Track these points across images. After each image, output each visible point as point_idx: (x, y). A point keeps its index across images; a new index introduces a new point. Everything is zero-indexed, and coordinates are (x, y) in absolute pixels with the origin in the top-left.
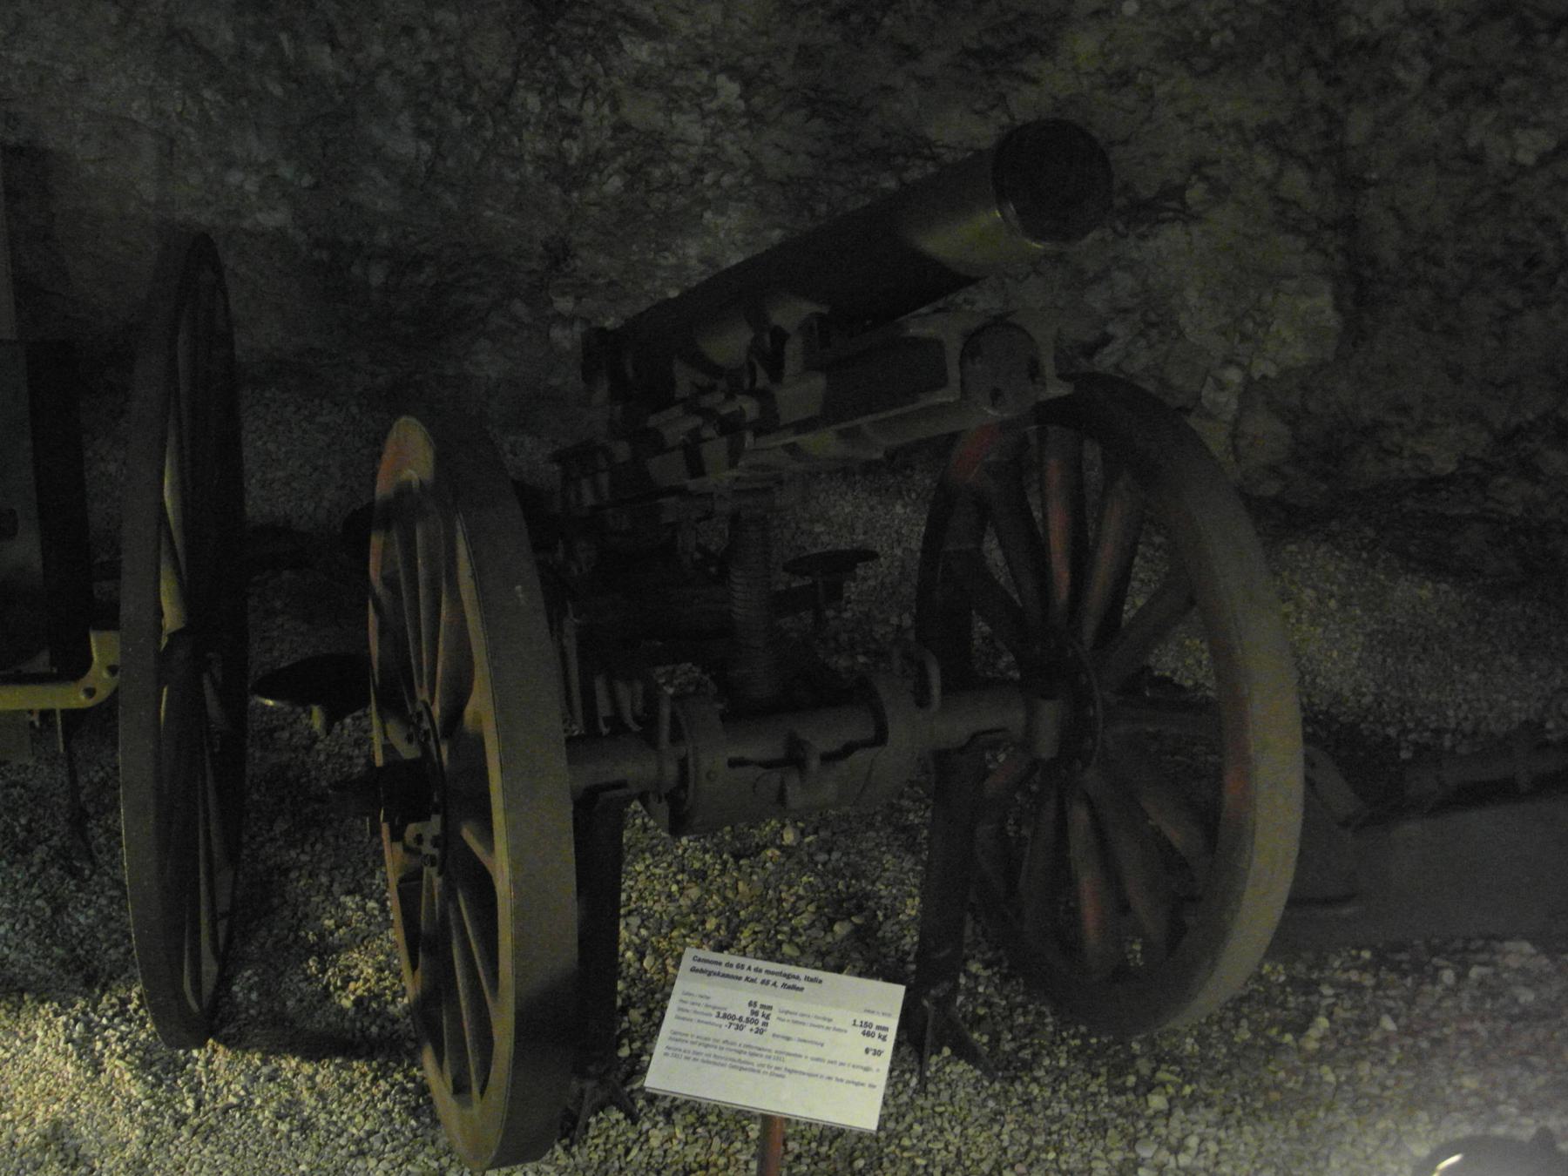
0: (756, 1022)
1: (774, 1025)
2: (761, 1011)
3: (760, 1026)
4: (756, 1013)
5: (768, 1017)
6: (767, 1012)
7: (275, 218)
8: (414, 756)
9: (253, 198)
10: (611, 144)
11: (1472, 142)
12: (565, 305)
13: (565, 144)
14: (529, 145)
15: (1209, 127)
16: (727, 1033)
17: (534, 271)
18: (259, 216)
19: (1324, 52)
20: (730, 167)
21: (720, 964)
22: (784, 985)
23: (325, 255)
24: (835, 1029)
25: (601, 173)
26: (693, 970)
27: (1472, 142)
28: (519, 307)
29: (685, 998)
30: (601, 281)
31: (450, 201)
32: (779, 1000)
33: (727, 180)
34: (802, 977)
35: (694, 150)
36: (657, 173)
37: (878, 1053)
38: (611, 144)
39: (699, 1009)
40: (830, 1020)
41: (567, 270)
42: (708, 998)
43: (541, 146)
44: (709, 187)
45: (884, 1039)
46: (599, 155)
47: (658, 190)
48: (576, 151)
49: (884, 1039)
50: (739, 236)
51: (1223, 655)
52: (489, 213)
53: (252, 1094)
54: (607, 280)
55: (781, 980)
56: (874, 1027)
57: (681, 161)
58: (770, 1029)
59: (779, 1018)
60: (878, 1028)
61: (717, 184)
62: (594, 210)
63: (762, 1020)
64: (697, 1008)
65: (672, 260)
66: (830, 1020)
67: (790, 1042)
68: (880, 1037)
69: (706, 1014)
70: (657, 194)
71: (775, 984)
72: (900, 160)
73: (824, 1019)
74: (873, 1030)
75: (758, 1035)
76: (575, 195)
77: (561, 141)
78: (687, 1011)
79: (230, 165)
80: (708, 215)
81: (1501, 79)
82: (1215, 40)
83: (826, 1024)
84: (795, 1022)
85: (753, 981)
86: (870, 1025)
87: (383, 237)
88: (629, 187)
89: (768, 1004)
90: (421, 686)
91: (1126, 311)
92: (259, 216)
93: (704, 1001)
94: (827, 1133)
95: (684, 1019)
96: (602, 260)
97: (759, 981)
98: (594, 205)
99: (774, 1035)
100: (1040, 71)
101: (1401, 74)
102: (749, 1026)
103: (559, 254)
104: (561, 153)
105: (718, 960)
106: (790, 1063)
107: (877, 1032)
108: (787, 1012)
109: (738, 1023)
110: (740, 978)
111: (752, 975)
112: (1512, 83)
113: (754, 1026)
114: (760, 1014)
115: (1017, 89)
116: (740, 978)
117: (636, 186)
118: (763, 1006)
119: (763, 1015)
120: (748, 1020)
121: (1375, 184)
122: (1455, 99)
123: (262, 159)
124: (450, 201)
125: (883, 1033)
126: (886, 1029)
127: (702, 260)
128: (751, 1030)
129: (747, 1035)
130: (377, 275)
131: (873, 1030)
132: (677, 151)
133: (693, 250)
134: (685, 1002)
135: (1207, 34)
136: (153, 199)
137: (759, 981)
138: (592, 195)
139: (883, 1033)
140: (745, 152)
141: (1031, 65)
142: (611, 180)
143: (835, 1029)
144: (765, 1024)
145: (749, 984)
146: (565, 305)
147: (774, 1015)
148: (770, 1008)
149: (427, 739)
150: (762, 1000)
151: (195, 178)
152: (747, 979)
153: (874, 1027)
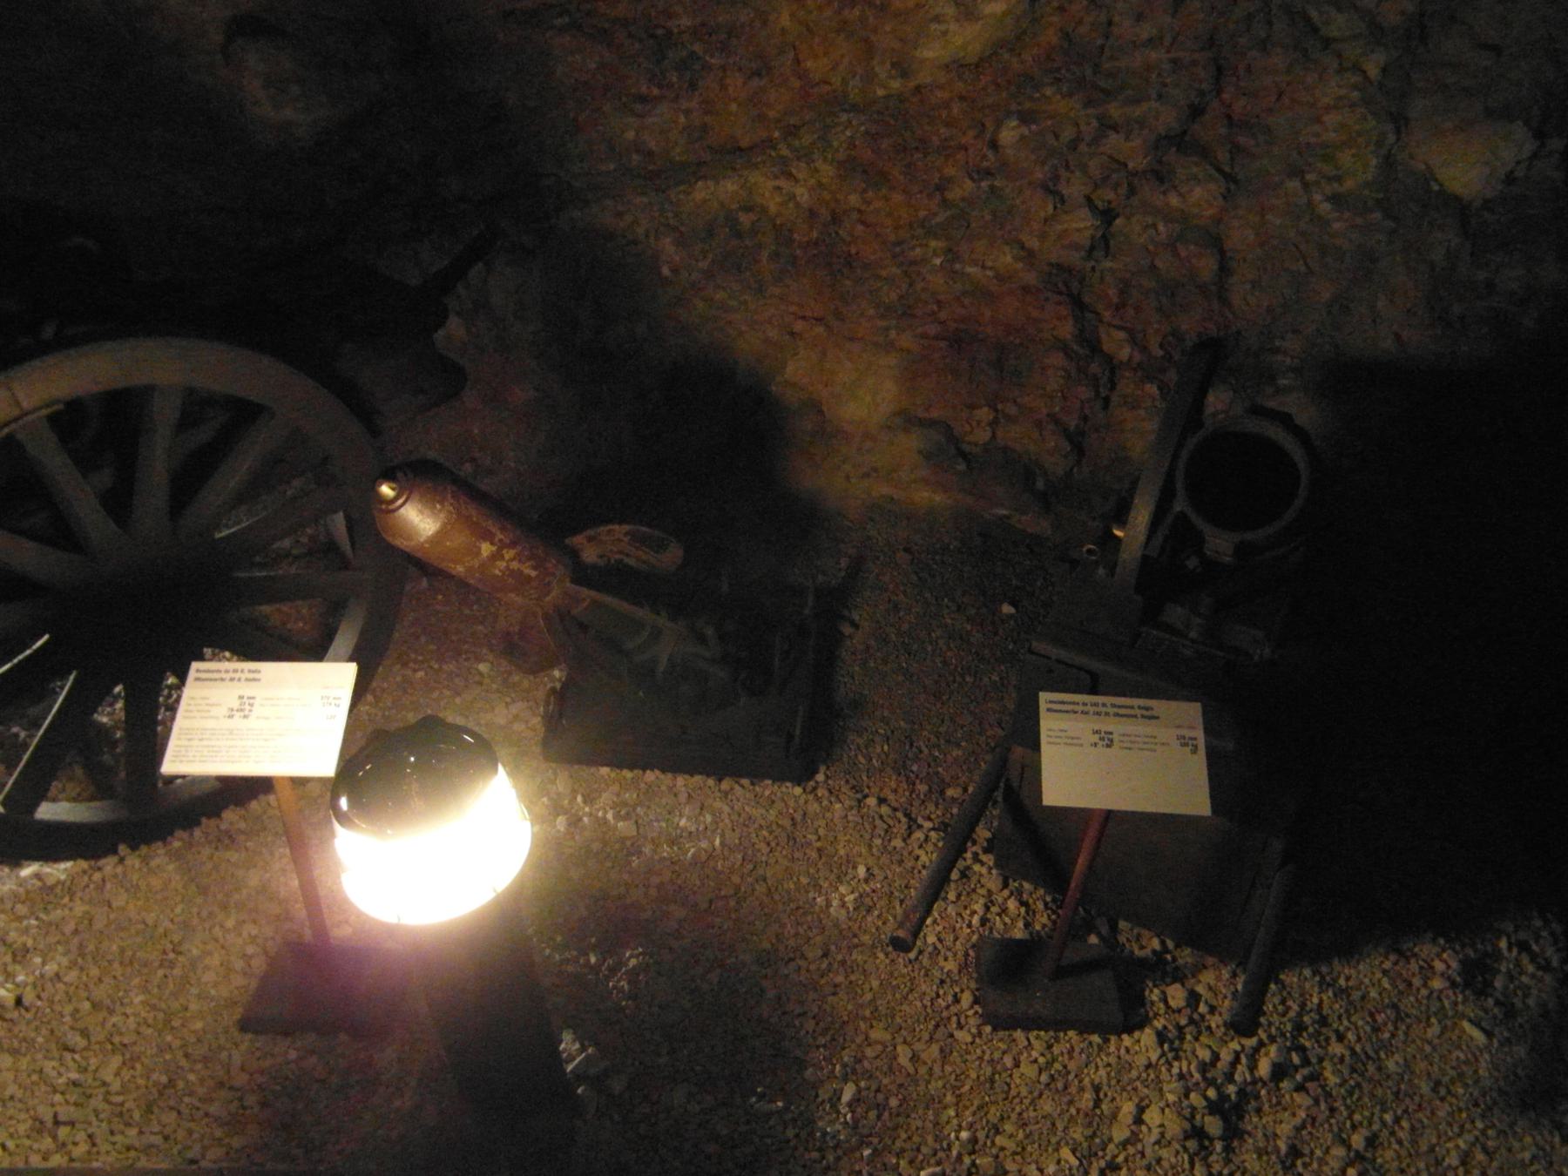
1: (257, 710)
3: (246, 713)
6: (251, 701)
8: (96, 819)
21: (1078, 704)
29: (1049, 733)
32: (247, 690)
37: (187, 711)
39: (200, 708)
40: (1155, 737)
51: (32, 535)
58: (254, 714)
63: (247, 707)
64: (200, 708)
66: (1155, 737)
73: (1151, 737)
83: (1152, 740)
84: (1128, 736)
85: (1087, 713)
86: (1184, 738)
89: (252, 695)
97: (243, 679)
102: (238, 714)
105: (1077, 701)
107: (1190, 742)
108: (266, 699)
113: (242, 714)
118: (1105, 733)
120: (237, 710)
125: (337, 702)
126: (1195, 739)
130: (872, 665)
134: (1051, 737)
145: (1096, 717)
147: (257, 702)
148: (1111, 733)
149: (874, 820)
150: (1104, 728)
152: (1082, 712)
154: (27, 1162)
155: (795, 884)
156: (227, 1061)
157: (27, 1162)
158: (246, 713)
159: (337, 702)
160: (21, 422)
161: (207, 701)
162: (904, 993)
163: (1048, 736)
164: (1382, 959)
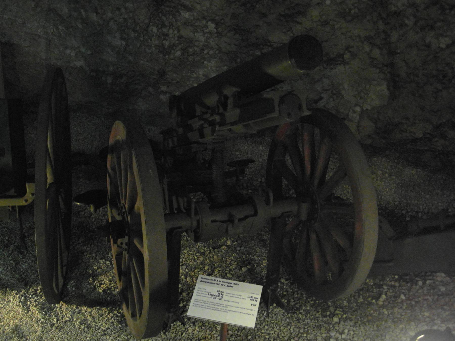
0: (219, 296)
2: (221, 293)
3: (220, 297)
4: (219, 294)
5: (223, 295)
6: (223, 293)
7: (80, 63)
9: (74, 57)
10: (177, 42)
11: (427, 41)
12: (164, 88)
13: (164, 42)
14: (154, 42)
15: (351, 37)
16: (211, 299)
17: (155, 79)
18: (75, 63)
19: (384, 15)
20: (212, 48)
21: (209, 279)
22: (228, 286)
23: (94, 74)
24: (242, 298)
25: (174, 50)
26: (201, 281)
27: (427, 41)
28: (151, 89)
29: (199, 289)
30: (174, 81)
31: (131, 58)
32: (226, 290)
33: (211, 52)
34: (233, 283)
35: (201, 44)
36: (191, 50)
37: (255, 305)
38: (177, 42)
39: (203, 293)
40: (241, 296)
41: (164, 78)
42: (205, 289)
43: (157, 42)
44: (206, 54)
45: (257, 301)
46: (174, 45)
47: (191, 55)
48: (167, 44)
49: (257, 301)
50: (214, 69)
52: (142, 62)
53: (73, 317)
54: (176, 81)
55: (227, 284)
56: (254, 298)
57: (198, 47)
58: (223, 298)
59: (226, 295)
60: (255, 298)
61: (208, 53)
62: (172, 61)
63: (221, 296)
65: (195, 76)
66: (241, 296)
67: (229, 302)
68: (255, 301)
69: (205, 294)
70: (191, 56)
71: (225, 285)
72: (261, 46)
73: (239, 295)
74: (253, 299)
75: (220, 300)
76: (167, 56)
78: (199, 293)
79: (67, 48)
80: (205, 62)
81: (435, 23)
82: (353, 12)
83: (240, 297)
84: (231, 296)
85: (219, 284)
86: (253, 297)
87: (111, 69)
88: (183, 54)
89: (223, 291)
90: (122, 199)
91: (327, 90)
92: (75, 63)
93: (204, 290)
94: (240, 328)
95: (198, 295)
96: (175, 75)
97: (220, 284)
98: (173, 59)
99: (225, 300)
100: (302, 21)
101: (407, 21)
102: (217, 298)
103: (162, 74)
104: (163, 44)
105: (208, 278)
106: (229, 308)
107: (255, 299)
108: (228, 294)
109: (214, 297)
110: (215, 284)
111: (218, 283)
112: (439, 24)
113: (219, 298)
114: (221, 294)
115: (295, 26)
116: (215, 284)
117: (185, 54)
119: (221, 294)
121: (399, 53)
122: (422, 29)
123: (76, 46)
124: (131, 58)
125: (256, 300)
126: (257, 298)
127: (204, 75)
128: (218, 299)
129: (217, 300)
130: (109, 80)
131: (253, 299)
132: (196, 44)
133: (201, 72)
134: (199, 291)
135: (350, 10)
136: (44, 58)
137: (220, 284)
138: (172, 57)
139: (256, 300)
140: (216, 44)
141: (299, 19)
142: (177, 52)
143: (242, 298)
144: (222, 297)
145: (217, 285)
146: (164, 88)
147: (225, 294)
148: (223, 292)
150: (221, 290)
151: (57, 52)
152: (217, 284)
153: (254, 298)
156: (227, 123)
162: (427, 132)
164: (439, 87)
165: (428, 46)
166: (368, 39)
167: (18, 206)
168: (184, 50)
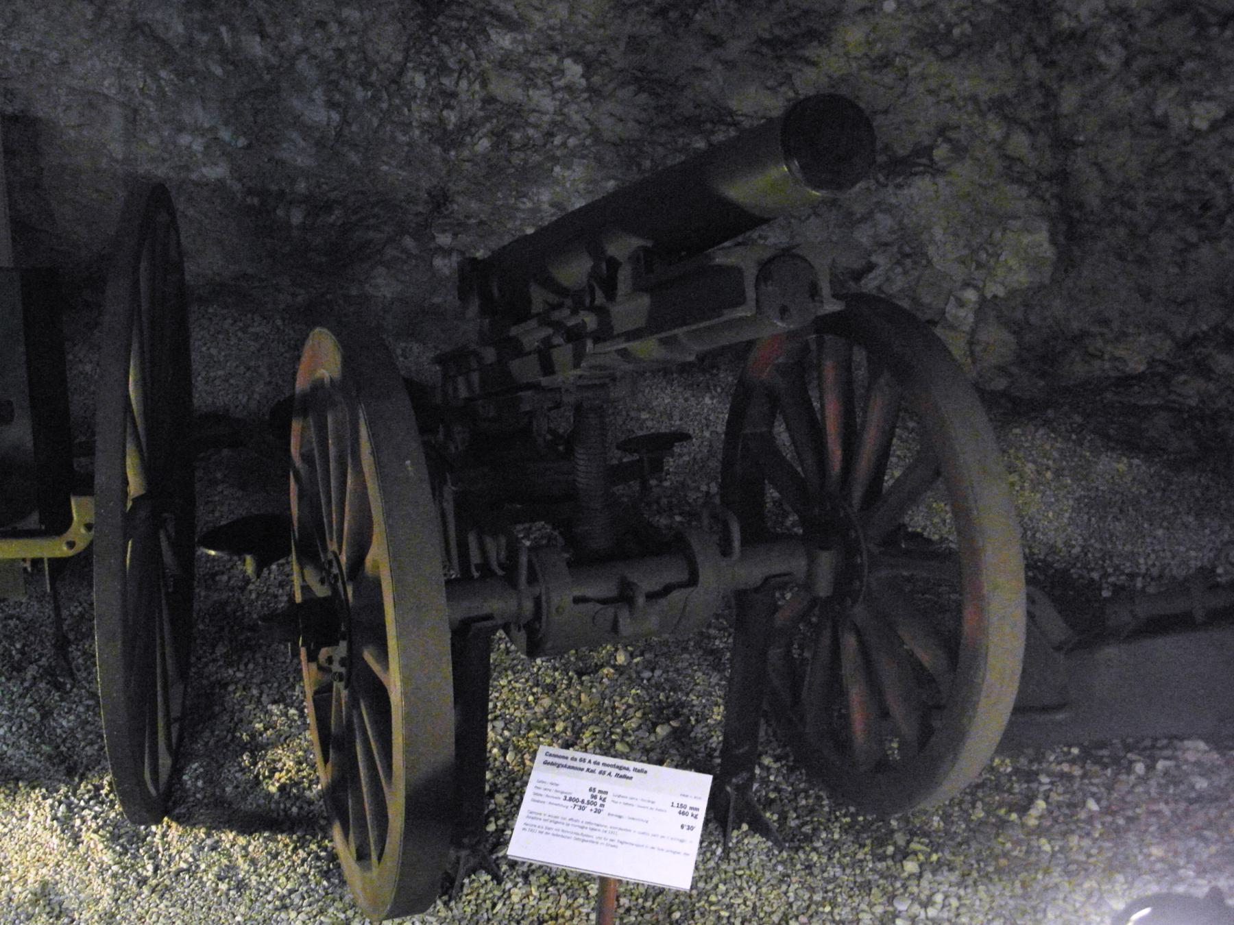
0: (595, 804)
6: (604, 796)
7: (216, 171)
10: (481, 114)
11: (1159, 112)
12: (444, 239)
14: (417, 115)
15: (951, 100)
16: (573, 812)
18: (204, 170)
19: (1042, 41)
20: (574, 131)
21: (567, 758)
23: (256, 201)
25: (473, 136)
27: (1159, 112)
28: (408, 242)
30: (473, 221)
31: (354, 158)
33: (572, 142)
35: (546, 118)
36: (517, 136)
38: (481, 114)
39: (550, 794)
40: (653, 803)
41: (446, 213)
43: (426, 115)
44: (558, 147)
45: (696, 817)
46: (471, 122)
47: (518, 149)
49: (696, 817)
50: (582, 186)
52: (385, 168)
54: (477, 220)
58: (606, 810)
61: (564, 144)
62: (468, 165)
63: (599, 802)
65: (529, 205)
66: (653, 803)
76: (453, 153)
77: (442, 111)
79: (181, 129)
80: (557, 169)
81: (1181, 62)
82: (956, 32)
83: (650, 805)
85: (593, 771)
87: (302, 186)
88: (495, 147)
89: (604, 790)
91: (886, 244)
92: (204, 170)
93: (554, 788)
94: (651, 891)
96: (474, 205)
97: (597, 772)
98: (468, 161)
101: (1103, 58)
102: (589, 807)
103: (440, 200)
106: (621, 836)
109: (580, 804)
111: (592, 767)
112: (1190, 65)
113: (593, 807)
115: (800, 70)
120: (589, 803)
122: (1146, 78)
123: (206, 125)
124: (354, 158)
125: (695, 813)
126: (697, 809)
129: (588, 815)
130: (297, 217)
132: (533, 118)
133: (545, 196)
134: (539, 788)
136: (120, 157)
137: (597, 772)
138: (466, 153)
141: (811, 52)
144: (602, 805)
146: (444, 239)
147: (609, 798)
151: (153, 140)
152: (588, 770)
154: (1134, 616)
155: (160, 78)
157: (1134, 616)
158: (598, 807)
159: (695, 813)
160: (157, 630)
161: (653, 806)
163: (536, 787)
165: (1161, 125)
166: (999, 105)
167: (49, 559)
168: (499, 136)
